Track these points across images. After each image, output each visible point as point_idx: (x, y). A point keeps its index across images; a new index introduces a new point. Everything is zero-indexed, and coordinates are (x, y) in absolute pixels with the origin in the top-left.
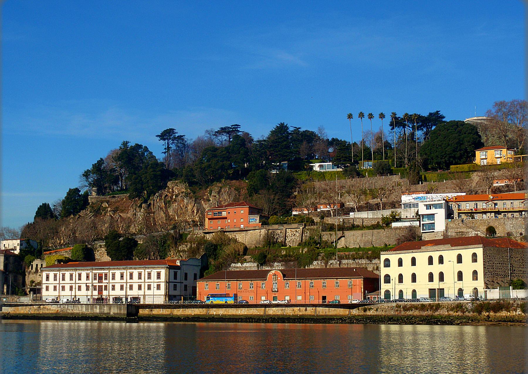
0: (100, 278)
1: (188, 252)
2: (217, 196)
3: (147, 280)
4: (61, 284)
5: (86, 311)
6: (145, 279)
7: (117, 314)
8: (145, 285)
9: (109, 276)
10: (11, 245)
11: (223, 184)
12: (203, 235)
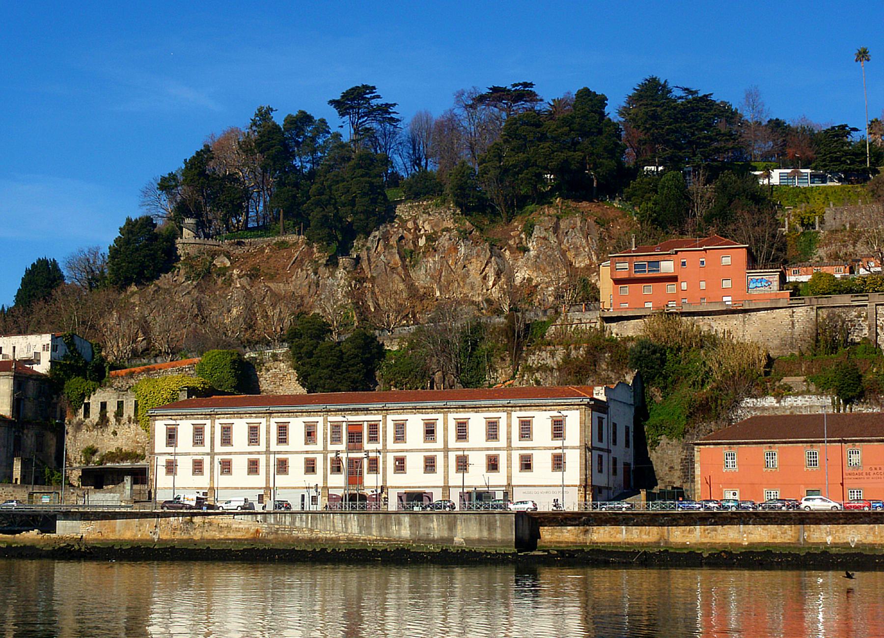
0: (355, 437)
1: (559, 369)
2: (553, 239)
3: (516, 442)
4: (219, 454)
5: (360, 532)
7: (480, 541)
8: (268, 461)
9: (385, 432)
11: (561, 209)
12: (598, 326)
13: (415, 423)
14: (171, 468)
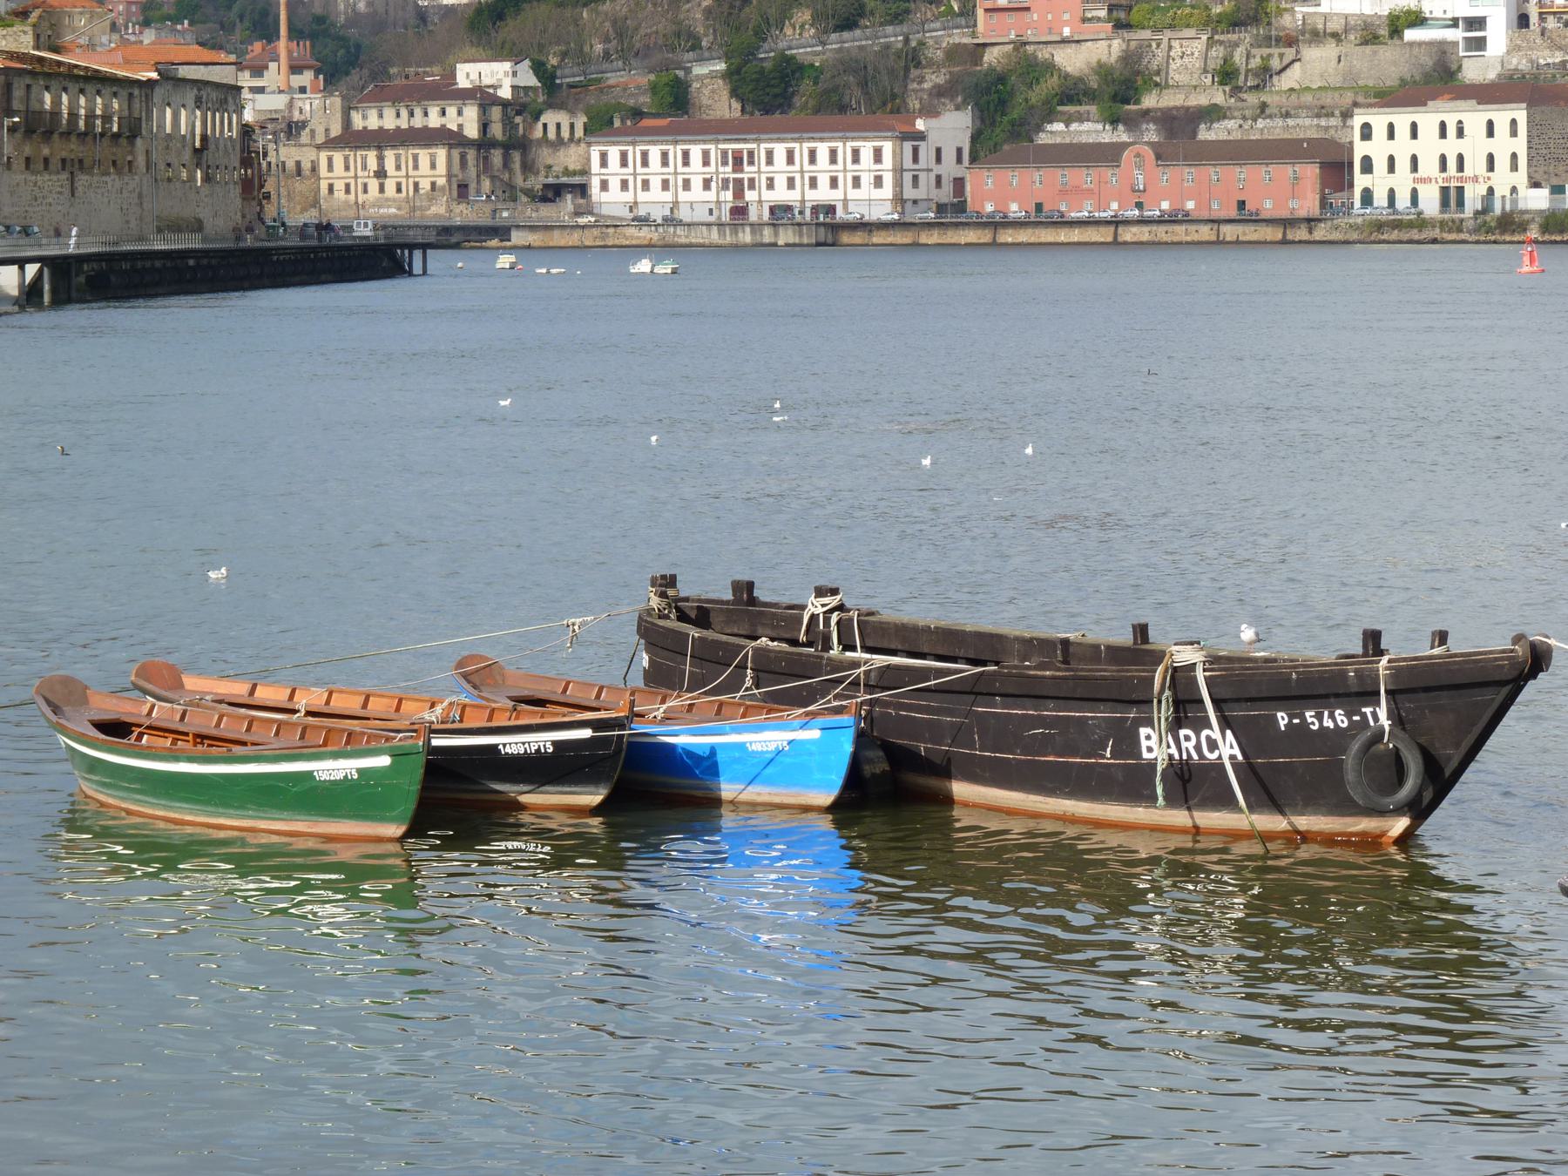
6: (845, 163)
10: (486, 76)
13: (780, 150)
14: (604, 186)
